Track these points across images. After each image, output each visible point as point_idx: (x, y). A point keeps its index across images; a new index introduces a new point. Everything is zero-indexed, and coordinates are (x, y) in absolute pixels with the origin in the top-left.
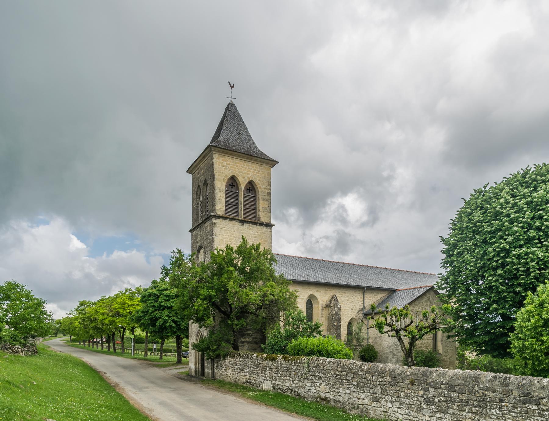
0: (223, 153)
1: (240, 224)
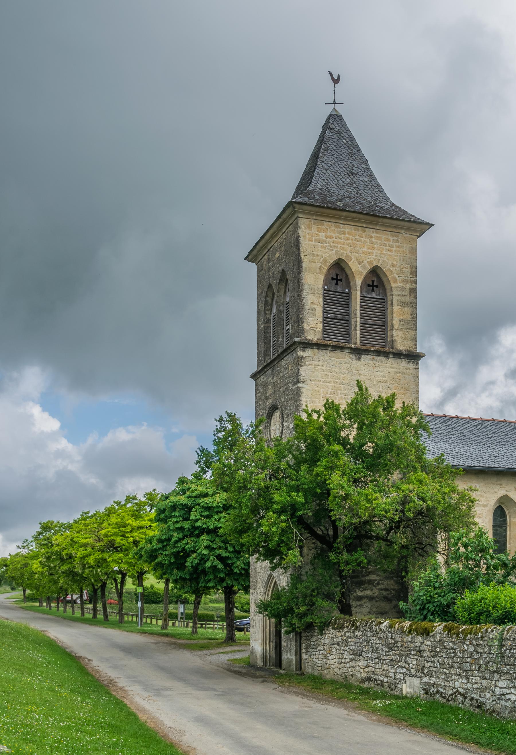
0: (317, 215)
1: (353, 356)
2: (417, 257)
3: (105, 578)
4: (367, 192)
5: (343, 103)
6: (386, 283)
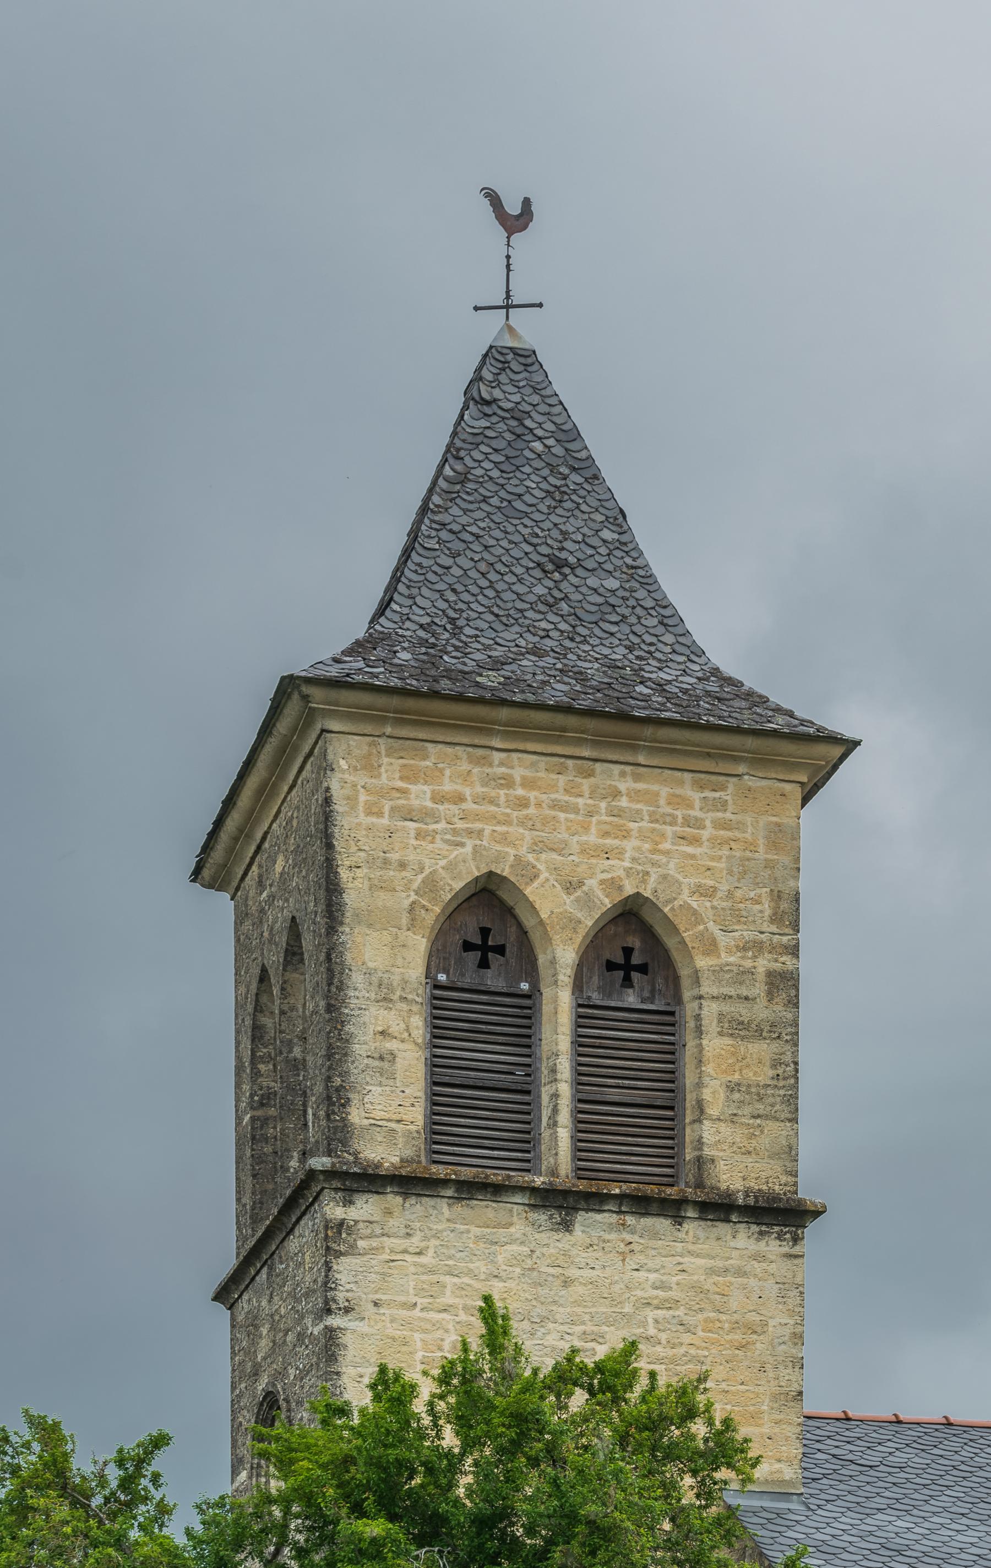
1: (541, 1217)
2: (797, 860)
4: (614, 629)
5: (540, 305)
6: (676, 956)
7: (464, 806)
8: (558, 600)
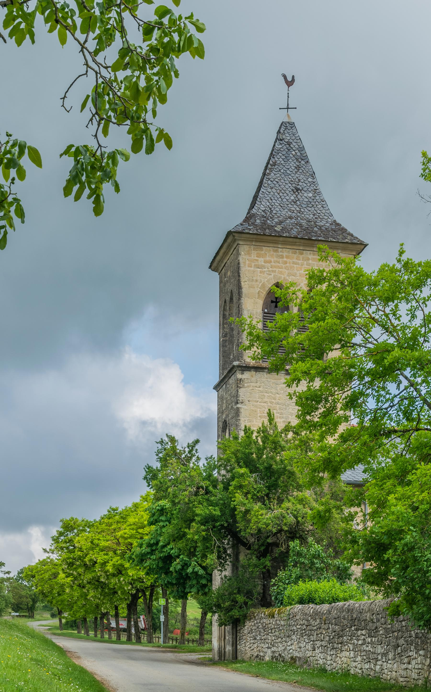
0: (256, 241)
3: (129, 588)
5: (296, 108)
7: (272, 264)
8: (297, 201)
